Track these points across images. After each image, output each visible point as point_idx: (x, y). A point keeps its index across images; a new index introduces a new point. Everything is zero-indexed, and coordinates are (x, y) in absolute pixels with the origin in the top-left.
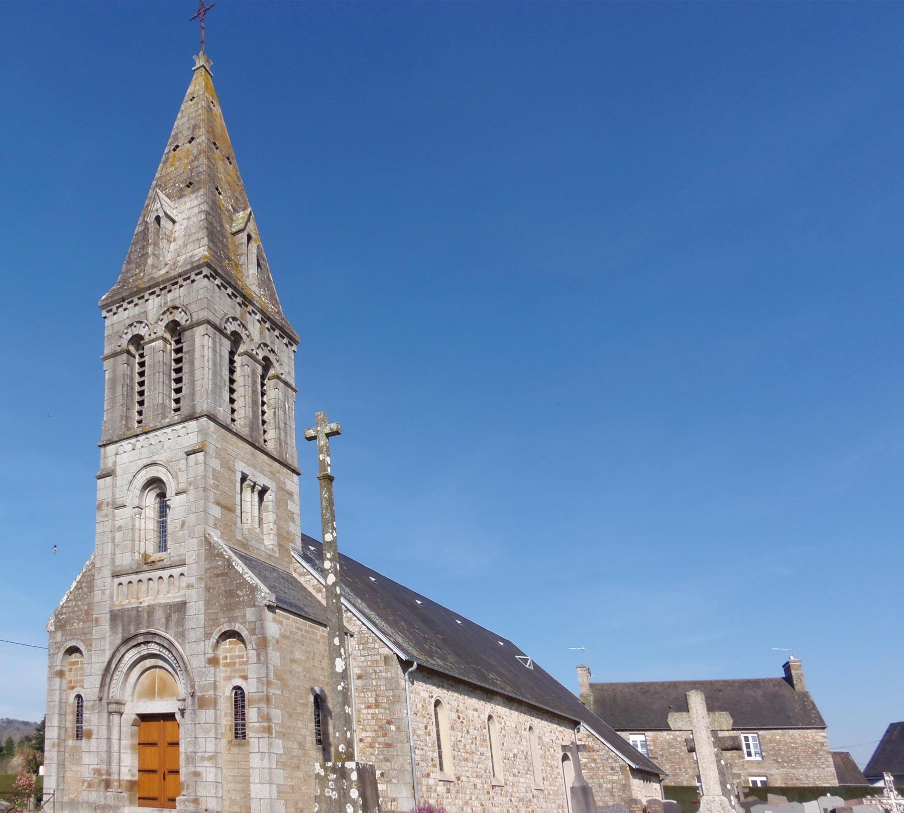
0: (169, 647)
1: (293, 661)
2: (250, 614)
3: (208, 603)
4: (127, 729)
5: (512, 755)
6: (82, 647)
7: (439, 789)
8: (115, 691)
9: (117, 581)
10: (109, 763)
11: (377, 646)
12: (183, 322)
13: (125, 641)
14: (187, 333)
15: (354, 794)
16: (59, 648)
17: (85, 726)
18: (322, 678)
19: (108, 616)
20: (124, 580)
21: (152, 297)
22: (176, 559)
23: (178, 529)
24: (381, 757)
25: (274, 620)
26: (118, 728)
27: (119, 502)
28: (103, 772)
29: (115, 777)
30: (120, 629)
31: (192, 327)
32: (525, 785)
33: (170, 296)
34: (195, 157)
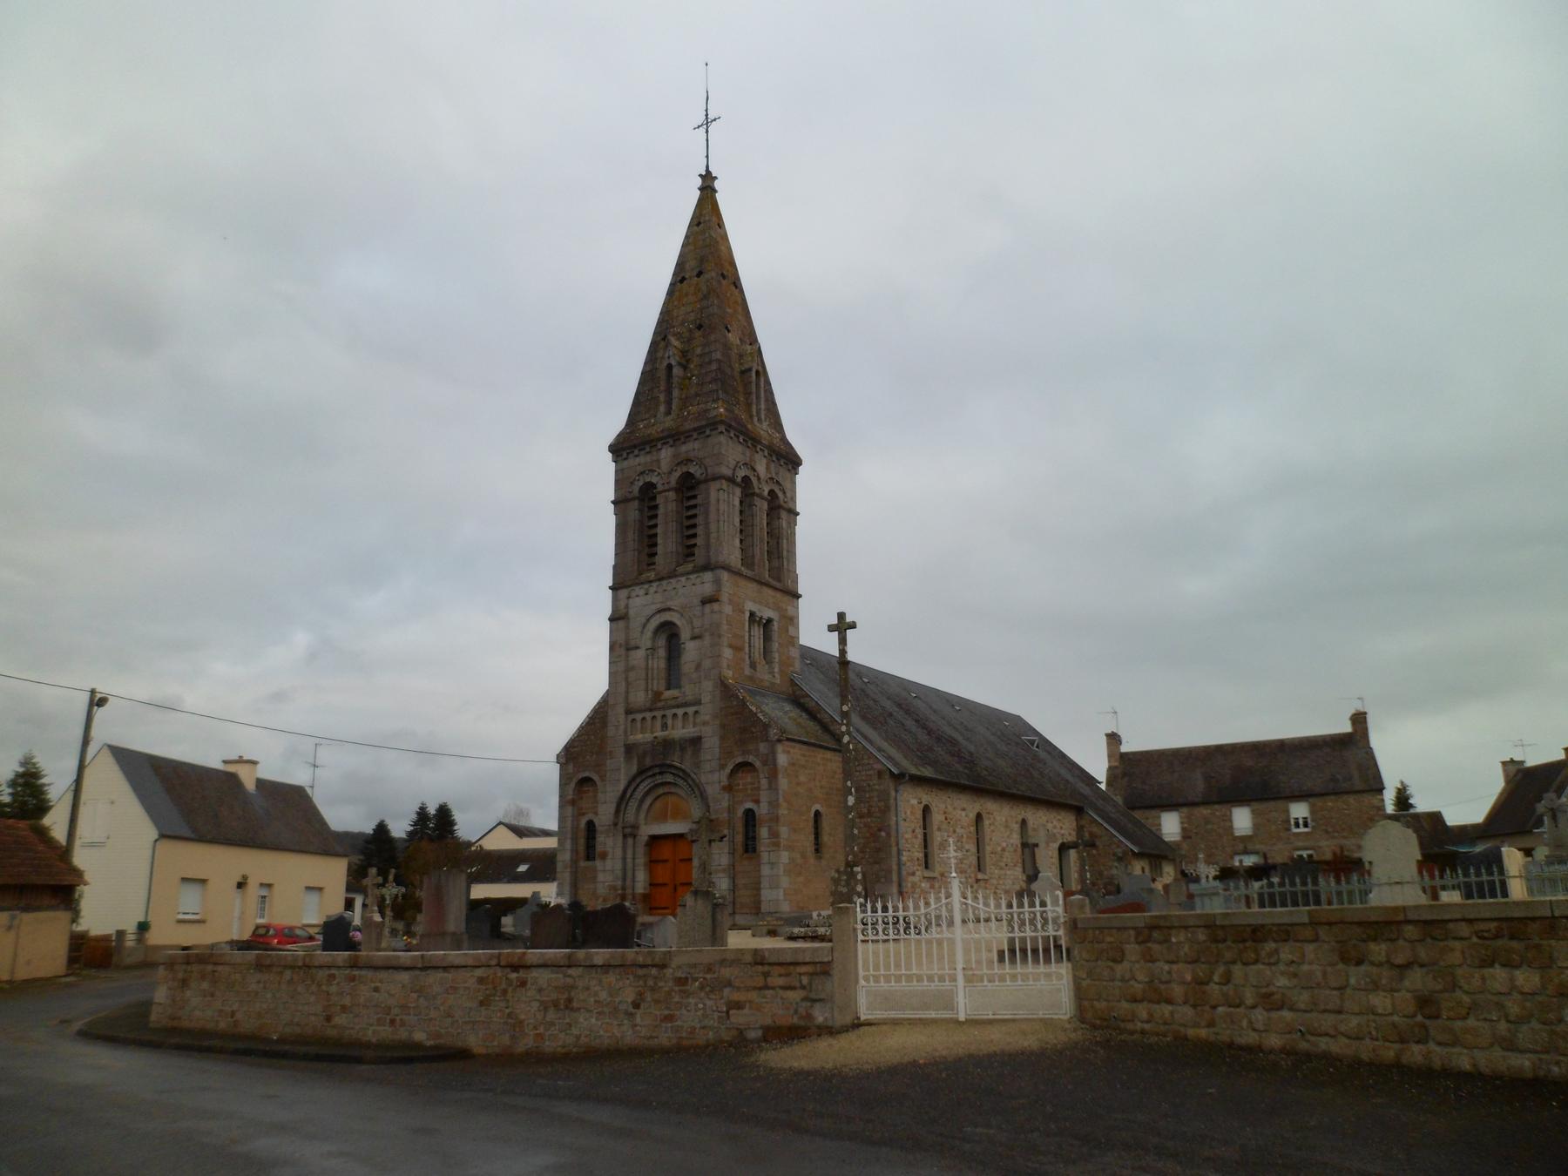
0: (685, 776)
1: (798, 784)
3: (722, 738)
4: (641, 850)
6: (596, 778)
8: (630, 816)
9: (631, 717)
10: (624, 879)
12: (698, 475)
13: (640, 773)
14: (703, 487)
15: (859, 888)
17: (599, 848)
20: (639, 717)
27: (632, 643)
29: (629, 891)
31: (706, 481)
33: (684, 448)
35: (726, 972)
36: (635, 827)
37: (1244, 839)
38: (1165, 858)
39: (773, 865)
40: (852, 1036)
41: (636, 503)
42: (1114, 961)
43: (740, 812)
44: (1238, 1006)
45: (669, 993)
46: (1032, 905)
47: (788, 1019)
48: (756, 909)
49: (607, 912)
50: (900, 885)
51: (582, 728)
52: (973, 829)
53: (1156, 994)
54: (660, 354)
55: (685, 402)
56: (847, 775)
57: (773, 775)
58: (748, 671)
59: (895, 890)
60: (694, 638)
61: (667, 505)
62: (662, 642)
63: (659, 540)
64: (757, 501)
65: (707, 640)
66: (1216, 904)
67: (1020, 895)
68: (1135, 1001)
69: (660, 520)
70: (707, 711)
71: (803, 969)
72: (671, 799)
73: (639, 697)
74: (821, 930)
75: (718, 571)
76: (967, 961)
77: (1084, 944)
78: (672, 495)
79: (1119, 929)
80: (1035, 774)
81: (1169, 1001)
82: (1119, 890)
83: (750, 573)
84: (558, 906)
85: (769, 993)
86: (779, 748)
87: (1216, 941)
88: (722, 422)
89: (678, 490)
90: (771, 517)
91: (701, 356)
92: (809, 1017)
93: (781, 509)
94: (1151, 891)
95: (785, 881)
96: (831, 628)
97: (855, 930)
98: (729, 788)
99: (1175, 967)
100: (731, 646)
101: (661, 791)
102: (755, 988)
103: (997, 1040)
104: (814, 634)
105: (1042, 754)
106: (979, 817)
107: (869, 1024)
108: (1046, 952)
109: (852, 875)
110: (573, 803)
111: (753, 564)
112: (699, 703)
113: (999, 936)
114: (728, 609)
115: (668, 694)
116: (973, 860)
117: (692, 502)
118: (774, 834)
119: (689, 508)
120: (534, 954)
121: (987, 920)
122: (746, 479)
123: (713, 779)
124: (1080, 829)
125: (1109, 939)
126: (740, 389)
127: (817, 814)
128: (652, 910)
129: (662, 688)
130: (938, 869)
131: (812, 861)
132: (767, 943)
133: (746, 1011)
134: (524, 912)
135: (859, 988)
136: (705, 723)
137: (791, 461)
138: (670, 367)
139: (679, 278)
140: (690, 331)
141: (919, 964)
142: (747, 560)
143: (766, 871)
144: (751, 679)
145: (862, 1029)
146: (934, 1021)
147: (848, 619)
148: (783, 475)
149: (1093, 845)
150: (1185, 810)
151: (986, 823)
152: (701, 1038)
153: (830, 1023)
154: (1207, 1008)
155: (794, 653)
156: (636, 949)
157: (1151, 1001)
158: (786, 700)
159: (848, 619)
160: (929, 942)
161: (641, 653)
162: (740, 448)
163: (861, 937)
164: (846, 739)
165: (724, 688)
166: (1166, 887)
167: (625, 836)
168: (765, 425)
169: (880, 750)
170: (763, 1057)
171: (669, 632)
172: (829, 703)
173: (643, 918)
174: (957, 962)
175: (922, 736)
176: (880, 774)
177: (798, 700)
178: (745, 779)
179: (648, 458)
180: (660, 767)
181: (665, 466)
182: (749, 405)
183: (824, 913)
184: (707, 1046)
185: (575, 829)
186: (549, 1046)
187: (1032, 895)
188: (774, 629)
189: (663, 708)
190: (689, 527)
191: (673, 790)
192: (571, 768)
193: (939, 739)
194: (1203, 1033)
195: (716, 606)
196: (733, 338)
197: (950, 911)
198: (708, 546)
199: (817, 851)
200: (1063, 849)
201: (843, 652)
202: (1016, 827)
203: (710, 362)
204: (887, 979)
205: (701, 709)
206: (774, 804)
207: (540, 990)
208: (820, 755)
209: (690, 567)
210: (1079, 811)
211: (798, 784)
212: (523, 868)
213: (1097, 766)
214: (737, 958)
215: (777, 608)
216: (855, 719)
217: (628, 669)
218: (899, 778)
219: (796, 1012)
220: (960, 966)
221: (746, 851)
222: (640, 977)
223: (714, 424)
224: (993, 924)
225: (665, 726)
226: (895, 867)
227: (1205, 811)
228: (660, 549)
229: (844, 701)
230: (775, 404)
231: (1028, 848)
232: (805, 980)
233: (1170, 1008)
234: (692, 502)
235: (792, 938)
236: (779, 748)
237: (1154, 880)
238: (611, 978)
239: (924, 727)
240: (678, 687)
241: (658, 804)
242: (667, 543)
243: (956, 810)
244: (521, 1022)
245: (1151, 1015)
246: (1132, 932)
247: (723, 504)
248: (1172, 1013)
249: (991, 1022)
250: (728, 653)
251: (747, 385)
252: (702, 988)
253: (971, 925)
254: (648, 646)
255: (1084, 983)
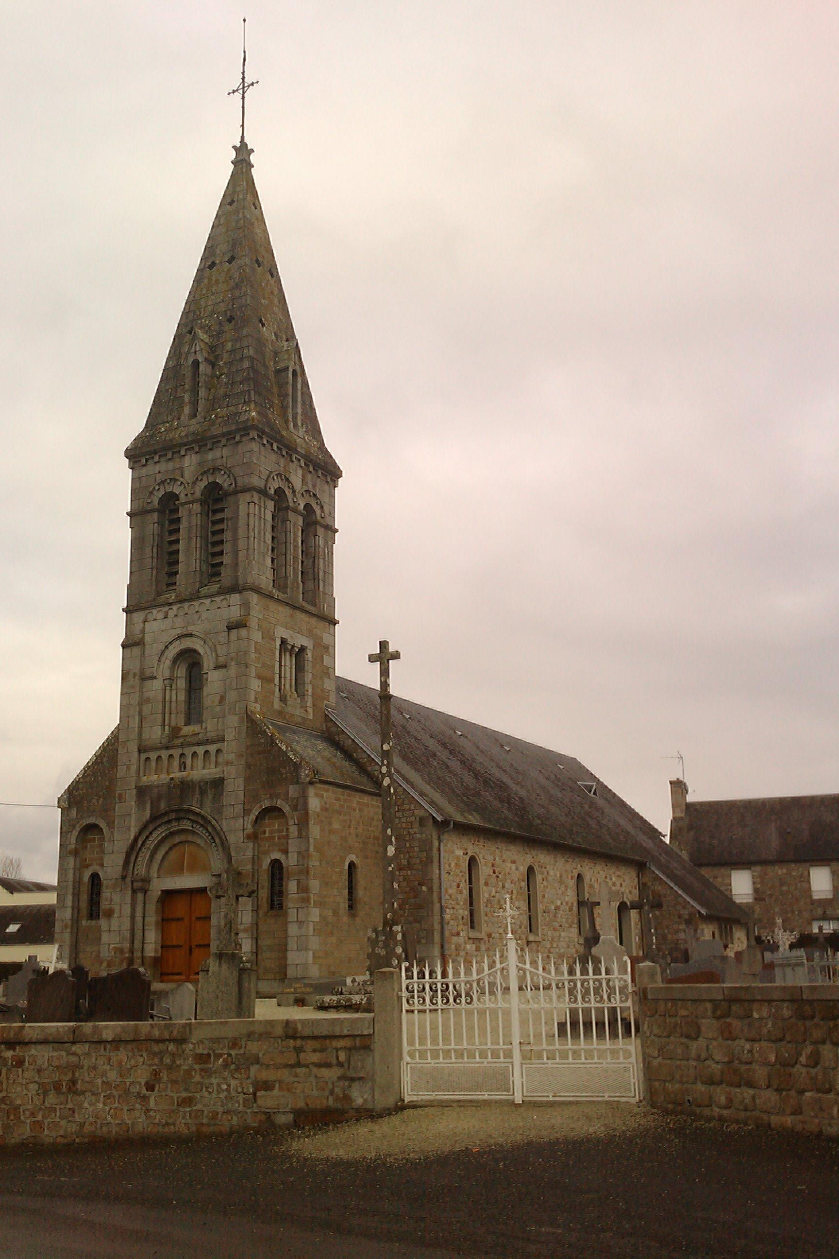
0: (205, 822)
1: (331, 832)
2: (293, 791)
3: (247, 780)
4: (152, 908)
5: (553, 908)
6: (103, 825)
7: (468, 947)
8: (141, 869)
9: (144, 756)
11: (412, 807)
13: (153, 818)
14: (231, 499)
15: (399, 950)
16: (74, 826)
17: (104, 905)
18: (357, 845)
19: (134, 792)
20: (153, 756)
21: (189, 452)
22: (213, 734)
23: (217, 702)
24: (411, 919)
25: (316, 795)
26: (142, 905)
27: (148, 673)
28: (126, 950)
29: (138, 954)
30: (148, 806)
31: (236, 492)
32: (567, 939)
33: (210, 456)
34: (237, 284)
35: (253, 1047)
36: (146, 880)
37: (824, 903)
38: (737, 922)
39: (300, 923)
40: (396, 1120)
41: (156, 515)
42: (688, 1037)
43: (266, 863)
44: (829, 1091)
45: (188, 1072)
46: (597, 971)
47: (321, 1100)
48: (282, 975)
49: (118, 978)
50: (442, 947)
51: (87, 768)
52: (524, 884)
53: (735, 1075)
54: (186, 348)
55: (213, 403)
56: (387, 821)
57: (303, 823)
58: (277, 705)
59: (437, 952)
60: (217, 668)
61: (191, 518)
62: (182, 671)
63: (181, 557)
64: (291, 514)
65: (233, 670)
66: (798, 975)
67: (584, 961)
68: (712, 1083)
69: (183, 534)
70: (232, 748)
71: (341, 1043)
72: (187, 848)
73: (155, 734)
74: (356, 999)
75: (246, 594)
76: (525, 1034)
77: (656, 1017)
78: (196, 507)
79: (694, 1001)
80: (593, 823)
81: (750, 1085)
82: (686, 959)
83: (281, 596)
84: (59, 973)
85: (300, 1071)
86: (311, 791)
87: (803, 1018)
88: (254, 427)
89: (203, 502)
90: (305, 531)
91: (232, 351)
92: (347, 1098)
93: (317, 525)
94: (724, 958)
95: (315, 943)
96: (372, 659)
97: (400, 998)
98: (254, 837)
99: (757, 1046)
100: (259, 677)
101: (177, 839)
102: (286, 1066)
103: (560, 1126)
104: (352, 663)
105: (600, 802)
106: (530, 870)
107: (414, 1106)
108: (612, 1025)
109: (391, 935)
110: (76, 853)
111: (286, 586)
112: (222, 740)
113: (558, 1006)
114: (257, 636)
115: (187, 730)
116: (526, 922)
117: (219, 516)
118: (304, 889)
119: (214, 523)
120: (34, 1029)
121: (548, 987)
122: (279, 492)
123: (235, 826)
124: (642, 887)
125: (683, 1012)
126: (275, 390)
127: (352, 865)
128: (163, 976)
129: (181, 722)
130: (485, 929)
131: (345, 919)
132: (298, 1014)
133: (276, 1092)
134: (19, 981)
135: (403, 1064)
136: (228, 763)
137: (328, 471)
138: (196, 364)
139: (208, 263)
140: (220, 323)
141: (471, 1038)
142: (279, 581)
143: (293, 930)
144: (280, 713)
145: (406, 1112)
146: (487, 1103)
147: (392, 649)
148: (320, 488)
149: (659, 906)
150: (758, 868)
151: (539, 877)
152: (227, 1123)
153: (370, 1106)
154: (793, 1093)
155: (329, 685)
156: (151, 1022)
157: (731, 1084)
158: (317, 737)
159: (392, 649)
160: (482, 1013)
161: (157, 684)
162: (274, 457)
163: (405, 1007)
164: (386, 781)
165: (253, 726)
166: (738, 954)
167: (134, 892)
168: (301, 431)
169: (422, 794)
170: (295, 1145)
171: (190, 660)
172: (366, 739)
173: (156, 986)
174: (510, 1037)
175: (469, 780)
176: (422, 821)
177: (333, 738)
178: (271, 827)
179: (171, 465)
180: (177, 812)
181: (188, 476)
182: (284, 408)
183: (360, 979)
184: (231, 1133)
185: (77, 883)
186: (48, 1136)
187: (597, 962)
188: (307, 658)
189: (182, 746)
190: (214, 544)
191: (190, 838)
192: (74, 812)
193: (486, 782)
194: (789, 1120)
195: (243, 632)
196: (267, 333)
197: (506, 978)
198: (236, 565)
199: (351, 907)
200: (623, 908)
201: (385, 685)
202: (572, 883)
203: (242, 359)
204: (435, 1054)
205: (224, 746)
206: (304, 855)
207: (39, 1071)
208: (357, 799)
209: (215, 588)
210: (640, 867)
211: (331, 832)
212: (13, 928)
213: (660, 816)
214: (267, 1031)
215: (310, 634)
216: (397, 760)
217: (144, 701)
218: (443, 826)
219: (332, 1092)
220: (516, 1041)
221: (272, 907)
222: (155, 1054)
223: (245, 429)
224: (554, 992)
225: (183, 766)
226: (437, 927)
227: (780, 871)
228: (181, 568)
229: (385, 739)
230: (313, 409)
231: (586, 906)
232: (342, 1056)
233: (751, 1092)
234: (219, 516)
235: (323, 1008)
236: (311, 791)
237: (726, 947)
238: (122, 1055)
239: (470, 769)
240: (200, 722)
241: (173, 855)
242: (190, 560)
243: (505, 863)
244: (17, 1108)
245: (730, 1100)
246: (709, 1005)
247: (254, 519)
248: (753, 1097)
249: (551, 1104)
250: (255, 685)
251: (282, 385)
252: (226, 1066)
253: (529, 993)
254: (166, 678)
255: (655, 1062)
